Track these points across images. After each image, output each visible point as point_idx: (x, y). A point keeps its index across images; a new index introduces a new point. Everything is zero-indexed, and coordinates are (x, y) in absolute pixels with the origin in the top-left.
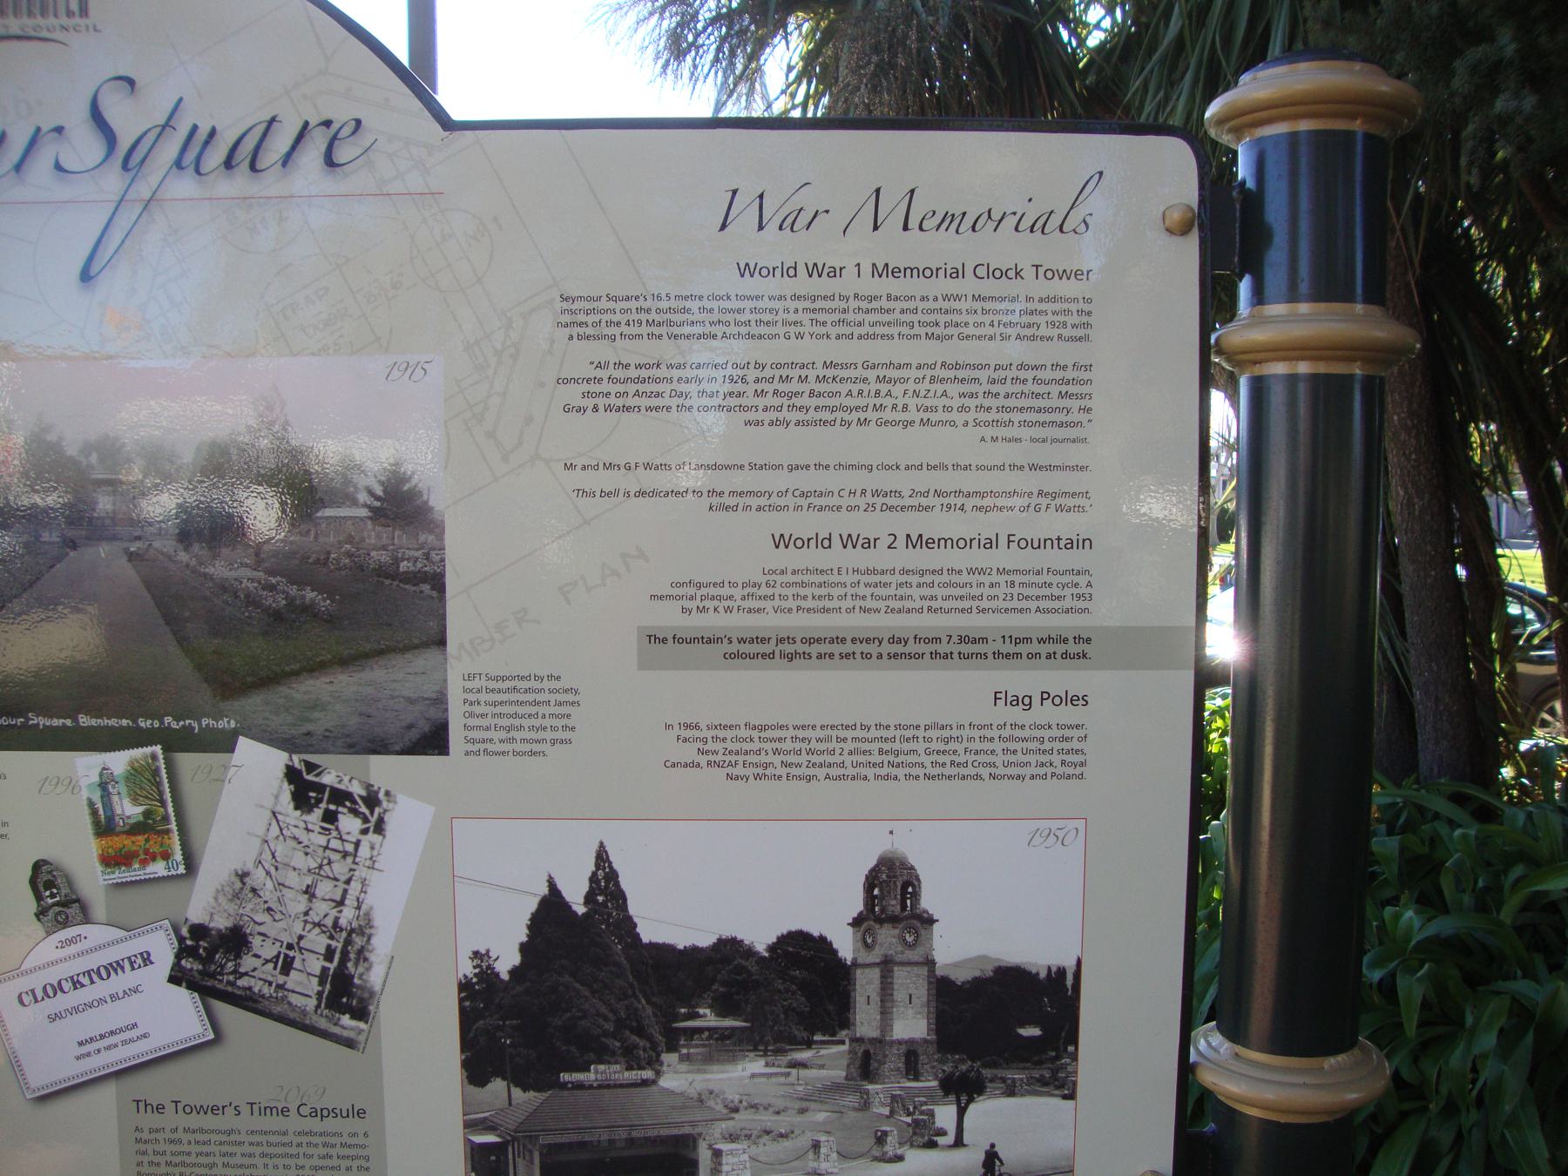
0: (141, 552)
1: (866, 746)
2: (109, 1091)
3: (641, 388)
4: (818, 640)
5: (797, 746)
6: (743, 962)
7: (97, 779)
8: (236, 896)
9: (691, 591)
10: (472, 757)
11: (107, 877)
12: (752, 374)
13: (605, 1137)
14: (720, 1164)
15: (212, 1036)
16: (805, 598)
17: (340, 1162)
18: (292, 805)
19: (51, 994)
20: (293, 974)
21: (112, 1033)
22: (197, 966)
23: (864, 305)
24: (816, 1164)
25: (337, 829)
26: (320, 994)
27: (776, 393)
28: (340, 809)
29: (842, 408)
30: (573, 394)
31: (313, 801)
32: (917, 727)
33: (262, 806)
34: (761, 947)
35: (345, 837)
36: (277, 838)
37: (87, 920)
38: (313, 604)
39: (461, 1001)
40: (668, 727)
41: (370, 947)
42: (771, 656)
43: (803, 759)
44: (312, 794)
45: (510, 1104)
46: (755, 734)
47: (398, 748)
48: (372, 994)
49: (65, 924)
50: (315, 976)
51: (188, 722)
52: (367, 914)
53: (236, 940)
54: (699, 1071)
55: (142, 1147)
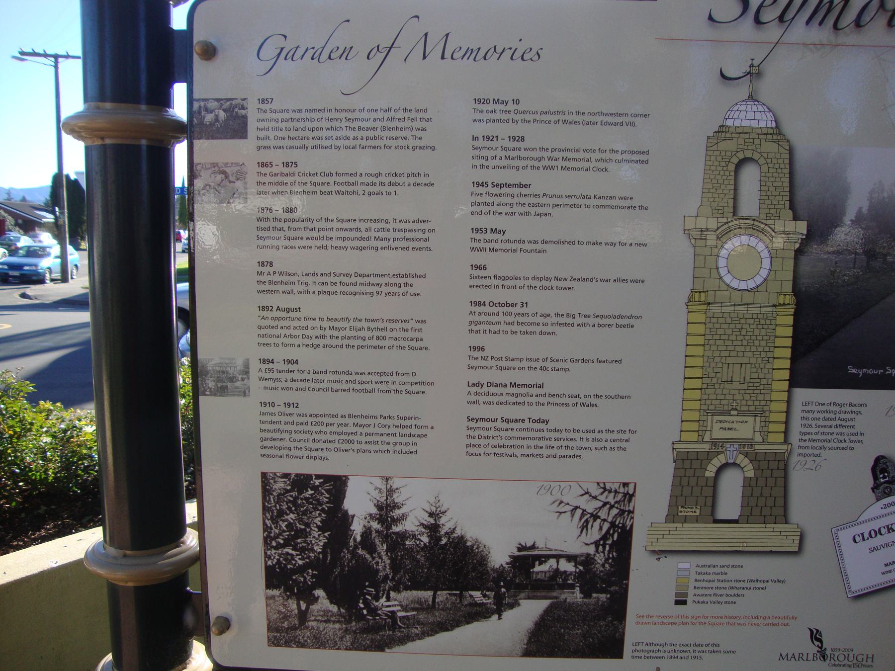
15: (797, 549)
19: (873, 536)
49: (889, 495)
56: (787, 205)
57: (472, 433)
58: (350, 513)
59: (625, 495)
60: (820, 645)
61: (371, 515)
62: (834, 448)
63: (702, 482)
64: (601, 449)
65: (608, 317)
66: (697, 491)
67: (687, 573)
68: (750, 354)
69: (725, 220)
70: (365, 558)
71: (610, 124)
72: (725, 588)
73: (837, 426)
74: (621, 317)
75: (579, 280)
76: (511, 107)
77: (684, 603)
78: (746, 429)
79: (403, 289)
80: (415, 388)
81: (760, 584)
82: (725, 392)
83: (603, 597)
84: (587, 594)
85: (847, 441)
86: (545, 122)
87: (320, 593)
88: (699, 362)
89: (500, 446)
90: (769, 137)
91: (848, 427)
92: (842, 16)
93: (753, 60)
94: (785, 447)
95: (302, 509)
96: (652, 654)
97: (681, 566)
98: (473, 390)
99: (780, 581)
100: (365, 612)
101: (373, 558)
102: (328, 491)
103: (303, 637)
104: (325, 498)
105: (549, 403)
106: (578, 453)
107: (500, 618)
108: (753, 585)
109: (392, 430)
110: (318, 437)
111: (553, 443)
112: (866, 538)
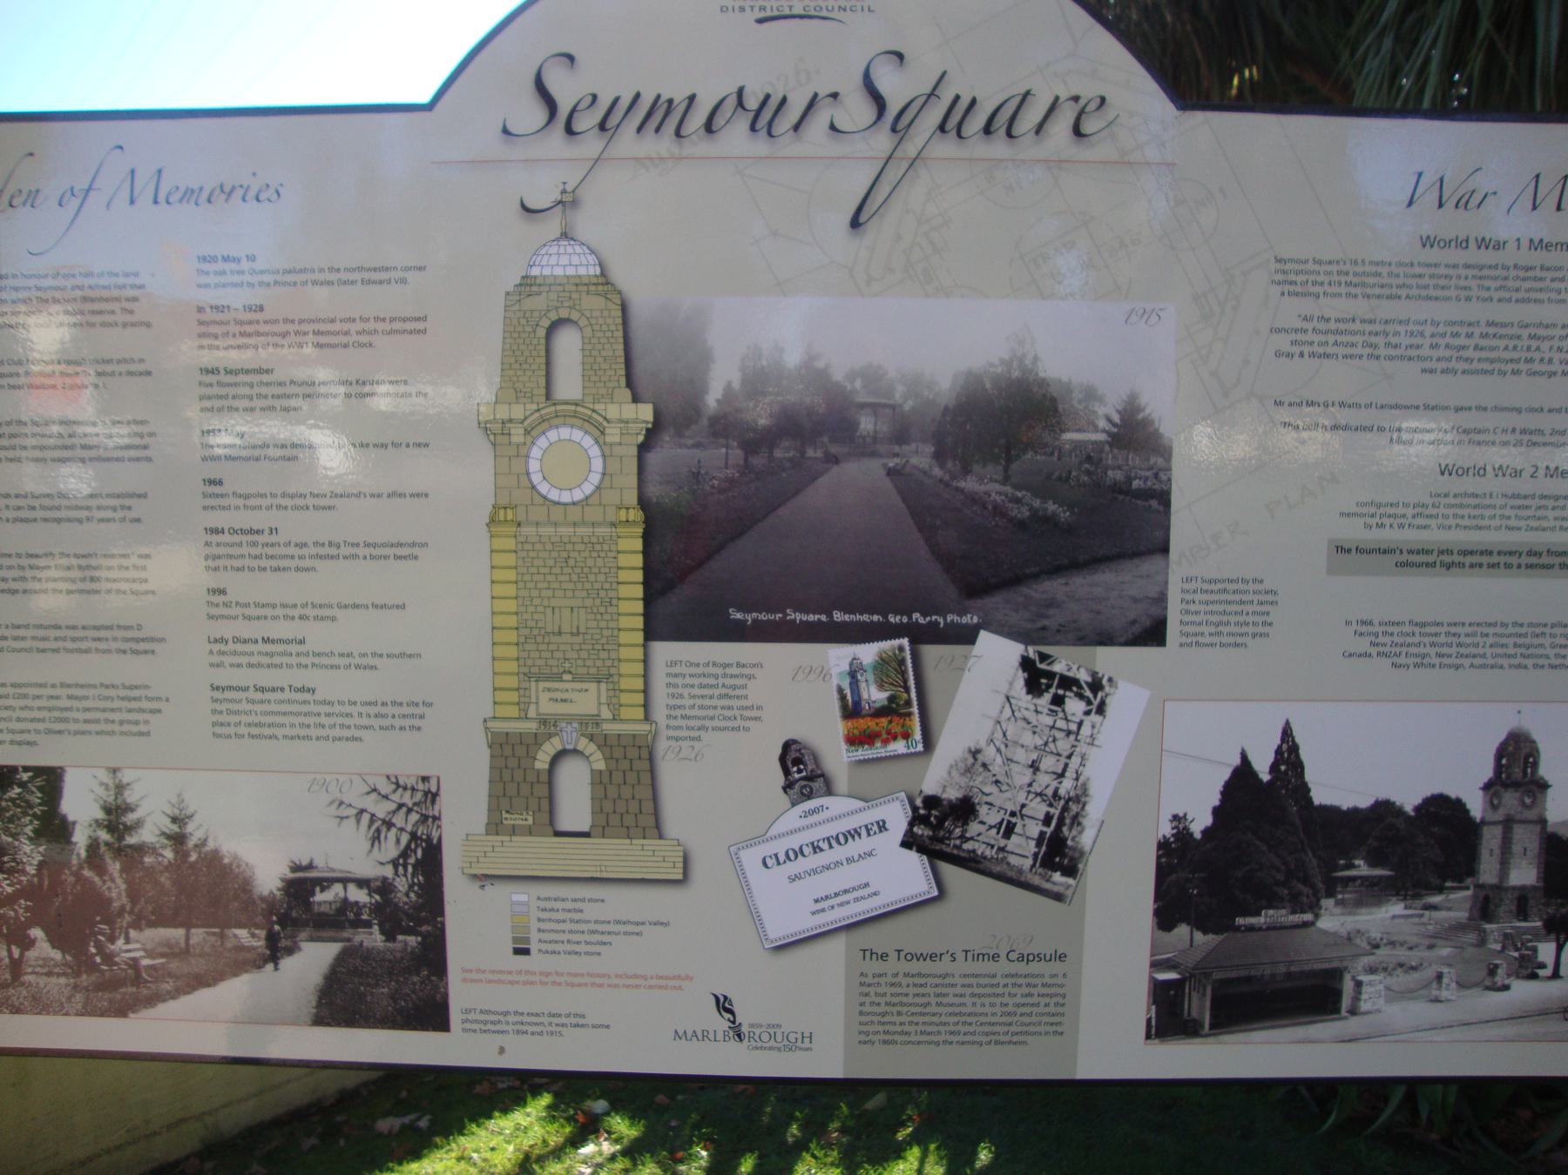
0: (898, 467)
1: (1504, 641)
2: (839, 944)
3: (1340, 338)
4: (1471, 553)
5: (1450, 639)
6: (1394, 820)
7: (847, 668)
8: (968, 770)
9: (1373, 510)
10: (1186, 649)
11: (851, 754)
12: (1428, 330)
13: (1268, 972)
14: (1360, 993)
15: (680, 877)
16: (1463, 517)
17: (1040, 999)
18: (1024, 690)
20: (1014, 837)
21: (846, 891)
22: (928, 832)
23: (1522, 274)
24: (1438, 992)
25: (1063, 711)
26: (1036, 855)
27: (1447, 346)
28: (1068, 693)
29: (1499, 360)
30: (1283, 342)
31: (1043, 687)
32: (1545, 625)
33: (997, 692)
34: (1409, 809)
35: (1069, 718)
36: (1009, 719)
37: (829, 792)
38: (1054, 514)
39: (1159, 857)
40: (1348, 623)
41: (1084, 813)
42: (1433, 565)
43: (1453, 650)
44: (1044, 681)
45: (1191, 945)
46: (1417, 630)
47: (1122, 640)
48: (1082, 854)
49: (809, 797)
50: (1033, 839)
51: (934, 618)
52: (1084, 785)
53: (965, 809)
54: (1350, 914)
55: (866, 990)
56: (623, 381)
57: (218, 707)
58: (71, 818)
59: (426, 793)
60: (732, 1019)
61: (97, 821)
62: (720, 729)
63: (531, 777)
64: (387, 728)
65: (384, 545)
66: (525, 789)
67: (524, 909)
68: (584, 594)
69: (535, 407)
70: (93, 882)
71: (374, 282)
72: (583, 932)
73: (721, 697)
74: (400, 545)
75: (342, 496)
76: (245, 265)
77: (526, 952)
78: (586, 700)
79: (120, 514)
80: (142, 646)
81: (633, 928)
82: (552, 647)
83: (412, 941)
84: (390, 936)
85: (739, 718)
86: (289, 284)
87: (37, 933)
88: (512, 606)
89: (256, 725)
90: (593, 288)
91: (738, 697)
92: (688, 116)
93: (565, 183)
94: (646, 727)
95: (7, 815)
96: (490, 1027)
97: (516, 898)
98: (216, 647)
99: (662, 924)
100: (98, 959)
101: (104, 882)
102: (40, 789)
103: (18, 998)
104: (36, 798)
105: (313, 665)
106: (357, 733)
107: (276, 969)
108: (621, 928)
109: (117, 704)
110: (24, 714)
111: (324, 720)
112: (781, 862)
